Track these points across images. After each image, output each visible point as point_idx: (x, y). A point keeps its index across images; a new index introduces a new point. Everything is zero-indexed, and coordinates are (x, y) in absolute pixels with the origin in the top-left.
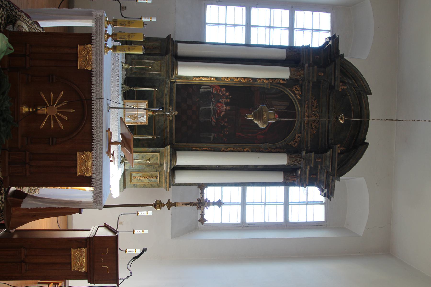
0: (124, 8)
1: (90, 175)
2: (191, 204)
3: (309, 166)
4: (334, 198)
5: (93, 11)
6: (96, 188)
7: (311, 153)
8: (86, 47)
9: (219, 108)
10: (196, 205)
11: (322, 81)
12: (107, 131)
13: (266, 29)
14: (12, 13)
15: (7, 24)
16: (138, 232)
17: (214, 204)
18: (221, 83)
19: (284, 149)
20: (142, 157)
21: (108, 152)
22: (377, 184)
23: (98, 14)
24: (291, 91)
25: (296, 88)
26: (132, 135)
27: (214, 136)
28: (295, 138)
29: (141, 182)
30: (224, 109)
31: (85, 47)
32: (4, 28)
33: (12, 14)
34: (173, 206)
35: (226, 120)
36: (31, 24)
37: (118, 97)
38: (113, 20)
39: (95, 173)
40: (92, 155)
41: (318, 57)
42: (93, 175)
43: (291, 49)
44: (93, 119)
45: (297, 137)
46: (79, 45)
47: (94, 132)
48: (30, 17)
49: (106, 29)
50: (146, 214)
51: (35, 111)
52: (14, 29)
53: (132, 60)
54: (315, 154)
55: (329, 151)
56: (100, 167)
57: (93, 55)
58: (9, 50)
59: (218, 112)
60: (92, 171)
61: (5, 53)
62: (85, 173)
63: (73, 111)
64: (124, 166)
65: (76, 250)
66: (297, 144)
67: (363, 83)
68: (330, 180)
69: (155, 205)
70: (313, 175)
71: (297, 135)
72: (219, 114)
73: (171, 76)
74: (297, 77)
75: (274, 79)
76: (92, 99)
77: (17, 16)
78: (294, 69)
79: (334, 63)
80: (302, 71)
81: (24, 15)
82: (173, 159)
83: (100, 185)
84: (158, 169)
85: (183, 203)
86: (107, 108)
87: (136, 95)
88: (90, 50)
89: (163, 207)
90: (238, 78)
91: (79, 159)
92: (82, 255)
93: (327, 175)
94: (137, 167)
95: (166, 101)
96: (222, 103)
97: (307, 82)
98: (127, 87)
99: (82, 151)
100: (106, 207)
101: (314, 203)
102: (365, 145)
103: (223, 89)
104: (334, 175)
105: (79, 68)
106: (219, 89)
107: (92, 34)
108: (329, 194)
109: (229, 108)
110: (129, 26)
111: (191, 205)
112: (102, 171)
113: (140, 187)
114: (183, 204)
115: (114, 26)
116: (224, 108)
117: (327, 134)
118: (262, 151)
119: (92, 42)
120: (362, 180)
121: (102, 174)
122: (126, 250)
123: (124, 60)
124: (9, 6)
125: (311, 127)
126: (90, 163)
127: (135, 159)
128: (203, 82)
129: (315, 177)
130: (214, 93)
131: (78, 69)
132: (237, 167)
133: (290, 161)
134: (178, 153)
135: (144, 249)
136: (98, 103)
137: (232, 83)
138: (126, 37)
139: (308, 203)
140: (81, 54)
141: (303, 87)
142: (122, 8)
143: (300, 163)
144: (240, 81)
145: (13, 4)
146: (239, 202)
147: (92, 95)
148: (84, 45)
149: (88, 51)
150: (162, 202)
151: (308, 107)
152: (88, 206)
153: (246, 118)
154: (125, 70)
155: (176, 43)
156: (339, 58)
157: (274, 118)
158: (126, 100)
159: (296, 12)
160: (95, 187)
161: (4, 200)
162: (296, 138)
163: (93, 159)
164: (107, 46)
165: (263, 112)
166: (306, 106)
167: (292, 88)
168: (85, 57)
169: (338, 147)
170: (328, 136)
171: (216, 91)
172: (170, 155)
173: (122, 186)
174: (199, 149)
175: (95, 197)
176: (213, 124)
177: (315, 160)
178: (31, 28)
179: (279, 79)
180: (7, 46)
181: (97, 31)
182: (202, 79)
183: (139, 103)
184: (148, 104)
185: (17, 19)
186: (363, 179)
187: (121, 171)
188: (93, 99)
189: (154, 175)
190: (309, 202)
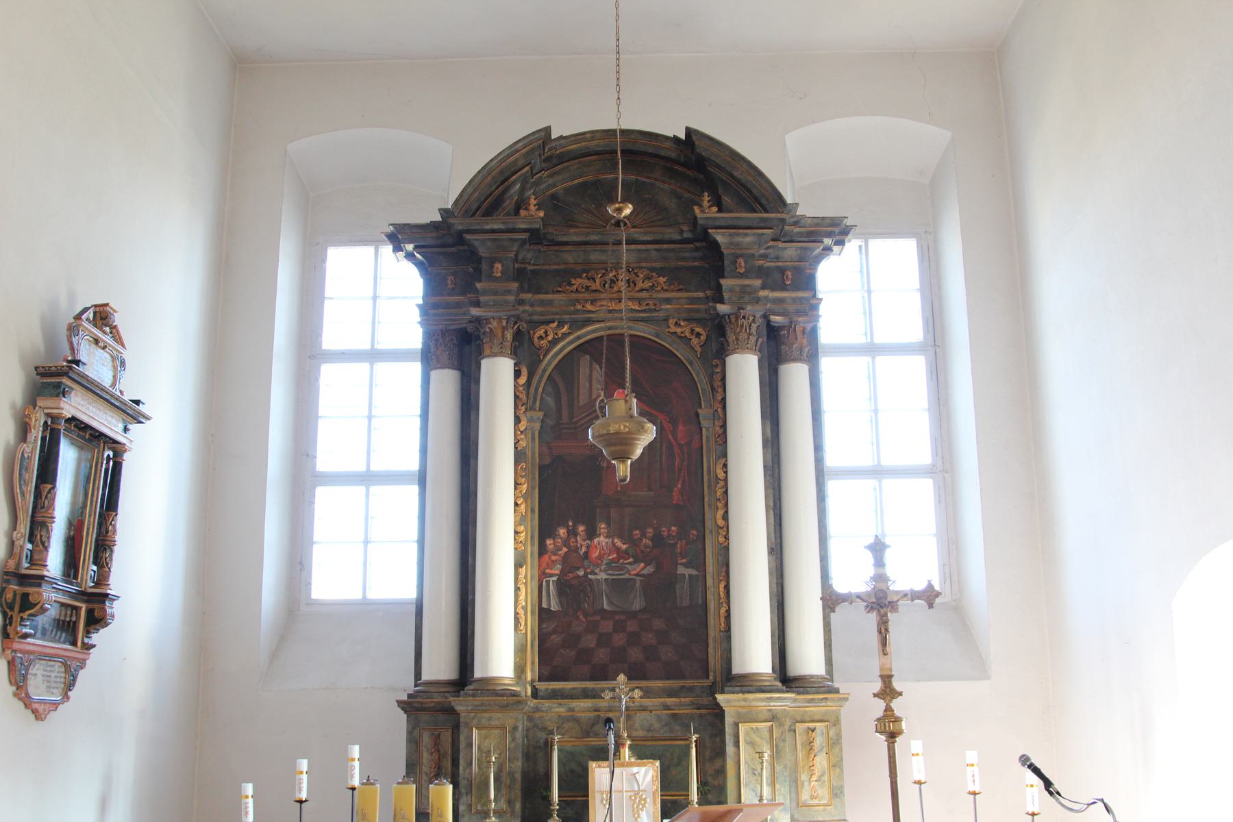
7: (724, 288)
10: (886, 615)
18: (531, 550)
25: (541, 338)
27: (686, 566)
34: (890, 682)
41: (450, 279)
45: (679, 330)
50: (921, 758)
54: (723, 277)
59: (614, 558)
66: (698, 330)
68: (797, 230)
71: (673, 329)
84: (787, 727)
106: (550, 558)
111: (887, 630)
117: (665, 246)
128: (532, 605)
134: (736, 670)
135: (1023, 765)
137: (532, 520)
141: (535, 318)
143: (751, 318)
151: (593, 302)
156: (451, 221)
157: (626, 401)
166: (589, 307)
176: (650, 569)
177: (741, 276)
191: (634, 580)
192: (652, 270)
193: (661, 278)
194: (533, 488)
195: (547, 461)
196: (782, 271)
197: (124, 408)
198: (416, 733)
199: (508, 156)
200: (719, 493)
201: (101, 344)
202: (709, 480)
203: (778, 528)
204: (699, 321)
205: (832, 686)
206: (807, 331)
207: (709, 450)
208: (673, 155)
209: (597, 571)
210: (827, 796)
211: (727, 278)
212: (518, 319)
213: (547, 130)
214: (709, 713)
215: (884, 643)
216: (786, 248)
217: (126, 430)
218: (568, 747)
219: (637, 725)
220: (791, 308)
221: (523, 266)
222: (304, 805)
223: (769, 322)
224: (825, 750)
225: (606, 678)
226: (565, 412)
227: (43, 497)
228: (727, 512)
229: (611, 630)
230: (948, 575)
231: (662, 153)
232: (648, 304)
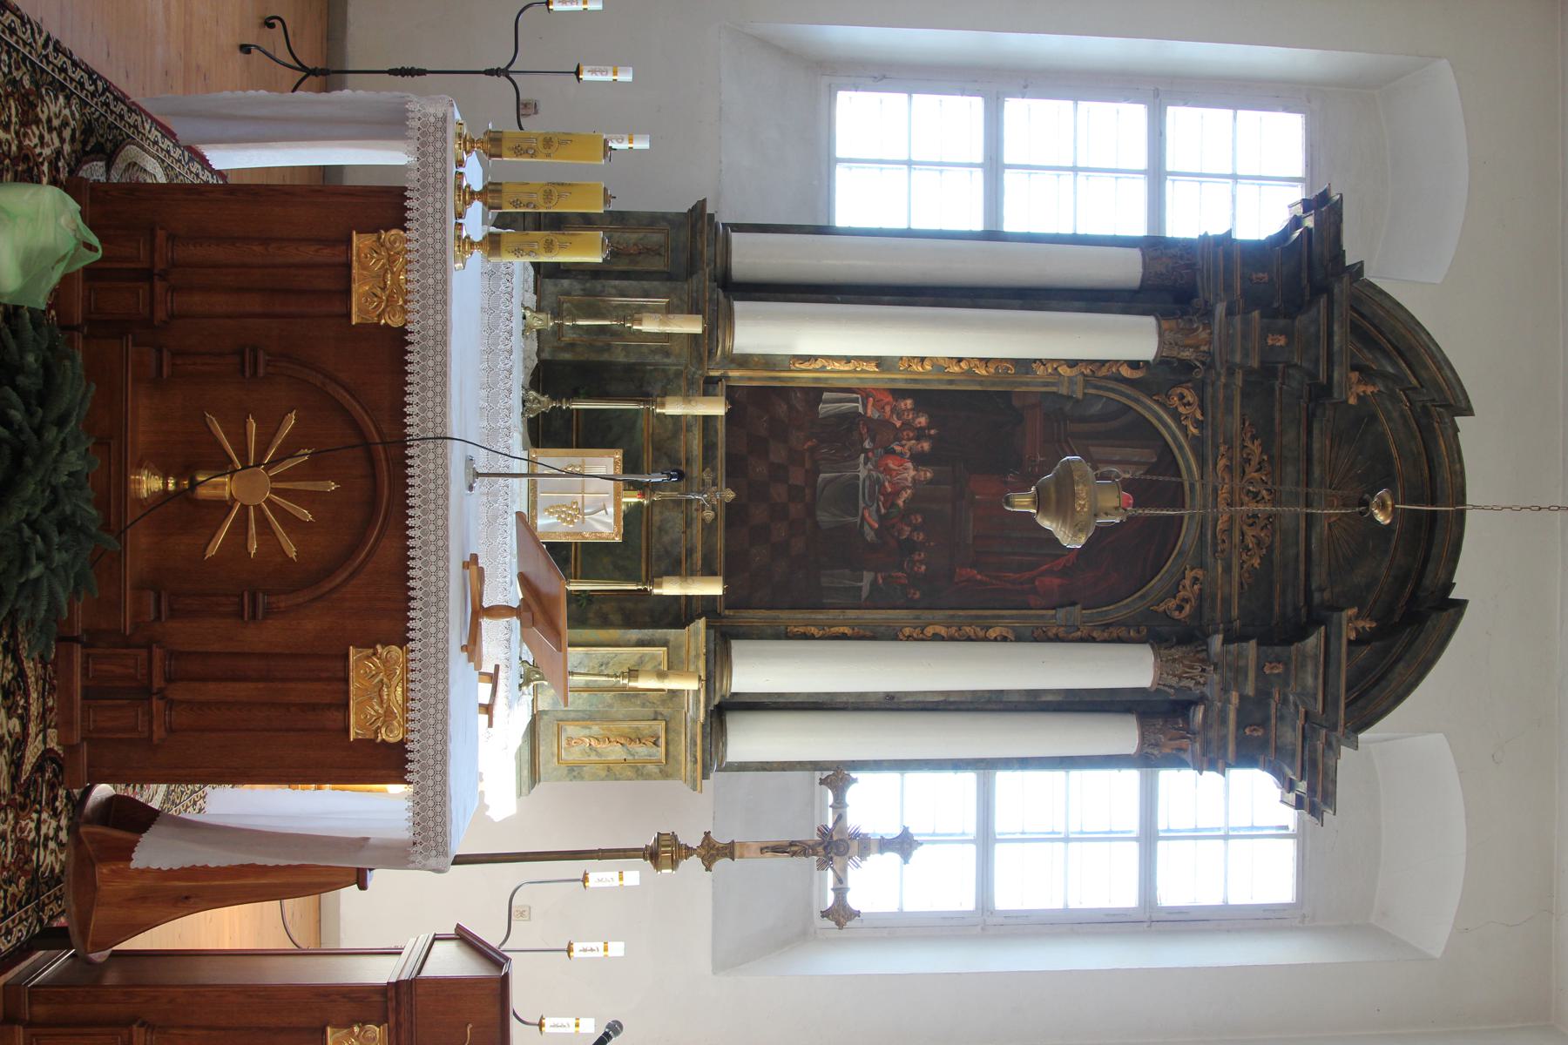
0: (528, 106)
1: (401, 736)
2: (794, 849)
3: (1237, 691)
4: (1335, 814)
5: (410, 101)
6: (423, 788)
7: (1244, 644)
8: (382, 240)
9: (891, 476)
10: (815, 854)
11: (1280, 366)
12: (466, 565)
13: (1058, 176)
14: (101, 114)
15: (81, 157)
16: (585, 950)
17: (885, 845)
18: (899, 379)
20: (602, 665)
21: (470, 648)
22: (1493, 756)
23: (431, 110)
25: (1182, 397)
26: (561, 579)
27: (874, 583)
28: (1181, 587)
29: (597, 758)
30: (910, 479)
31: (380, 238)
32: (71, 172)
33: (103, 119)
34: (725, 855)
35: (917, 520)
36: (179, 161)
38: (485, 134)
39: (419, 731)
40: (408, 661)
41: (1265, 276)
42: (410, 736)
43: (1154, 247)
44: (411, 517)
45: (1187, 582)
46: (354, 233)
47: (413, 568)
48: (175, 130)
49: (461, 170)
50: (616, 883)
51: (187, 487)
52: (112, 177)
53: (562, 298)
54: (1259, 644)
55: (1315, 635)
57: (410, 271)
58: (87, 251)
59: (885, 487)
60: (407, 720)
61: (69, 265)
62: (379, 728)
63: (333, 486)
64: (533, 700)
65: (345, 1031)
66: (1188, 607)
67: (1440, 372)
68: (1320, 745)
69: (652, 855)
70: (1251, 725)
71: (1189, 574)
73: (709, 357)
74: (1187, 354)
75: (1098, 364)
76: (408, 438)
77: (125, 126)
78: (1175, 321)
79: (1325, 296)
80: (1204, 329)
81: (151, 128)
82: (718, 669)
83: (438, 778)
84: (660, 709)
85: (763, 846)
86: (466, 475)
87: (577, 430)
88: (399, 249)
89: (684, 863)
90: (960, 360)
91: (358, 672)
93: (1306, 725)
94: (581, 701)
95: (688, 451)
96: (902, 454)
97: (1223, 371)
98: (542, 399)
99: (368, 642)
100: (460, 860)
101: (1253, 833)
102: (1452, 611)
103: (906, 405)
104: (1334, 727)
106: (888, 403)
107: (405, 189)
108: (1316, 799)
109: (928, 475)
110: (548, 156)
111: (794, 854)
112: (445, 723)
113: (595, 777)
114: (762, 849)
115: (491, 156)
117: (1302, 568)
118: (1056, 635)
119: (406, 220)
120: (1436, 743)
121: (445, 732)
122: (541, 1020)
123: (531, 300)
124: (92, 88)
125: (1243, 541)
126: (399, 689)
127: (572, 673)
128: (827, 379)
129: (1260, 734)
130: (870, 417)
131: (354, 323)
132: (963, 699)
133: (1165, 675)
134: (736, 646)
135: (609, 1026)
136: (431, 456)
137: (940, 381)
138: (538, 198)
139: (1231, 833)
140: (364, 267)
141: (1209, 390)
142: (521, 106)
143: (1202, 680)
144: (970, 373)
145: (106, 81)
146: (966, 832)
148: (376, 230)
149: (389, 254)
150: (682, 840)
151: (1229, 468)
152: (399, 856)
153: (1008, 509)
154: (535, 335)
155: (727, 232)
156: (1346, 279)
157: (1116, 508)
158: (538, 447)
159: (1171, 110)
160: (418, 783)
161: (68, 834)
162: (1184, 587)
163: (412, 676)
164: (464, 234)
165: (1073, 483)
166: (1222, 463)
167: (1168, 397)
168: (379, 276)
169: (1350, 620)
170: (1308, 575)
171: (878, 410)
172: (707, 654)
173: (526, 773)
174: (815, 633)
175: (419, 824)
176: (870, 535)
177: (1260, 668)
178: (177, 177)
179: (1118, 361)
180: (75, 236)
181: (424, 175)
182: (824, 367)
183: (588, 459)
184: (620, 464)
185: (124, 139)
186: (1439, 738)
187: (523, 717)
188: (410, 440)
189: (646, 732)
190: (1234, 829)
192: (1270, 549)
193: (1258, 561)
194: (981, 383)
195: (1016, 403)
196: (1264, 723)
199: (1433, 357)
203: (920, 706)
205: (711, 769)
208: (1427, 582)
209: (870, 466)
211: (1258, 649)
212: (1209, 366)
216: (1294, 730)
220: (1213, 734)
224: (629, 758)
225: (728, 475)
228: (943, 639)
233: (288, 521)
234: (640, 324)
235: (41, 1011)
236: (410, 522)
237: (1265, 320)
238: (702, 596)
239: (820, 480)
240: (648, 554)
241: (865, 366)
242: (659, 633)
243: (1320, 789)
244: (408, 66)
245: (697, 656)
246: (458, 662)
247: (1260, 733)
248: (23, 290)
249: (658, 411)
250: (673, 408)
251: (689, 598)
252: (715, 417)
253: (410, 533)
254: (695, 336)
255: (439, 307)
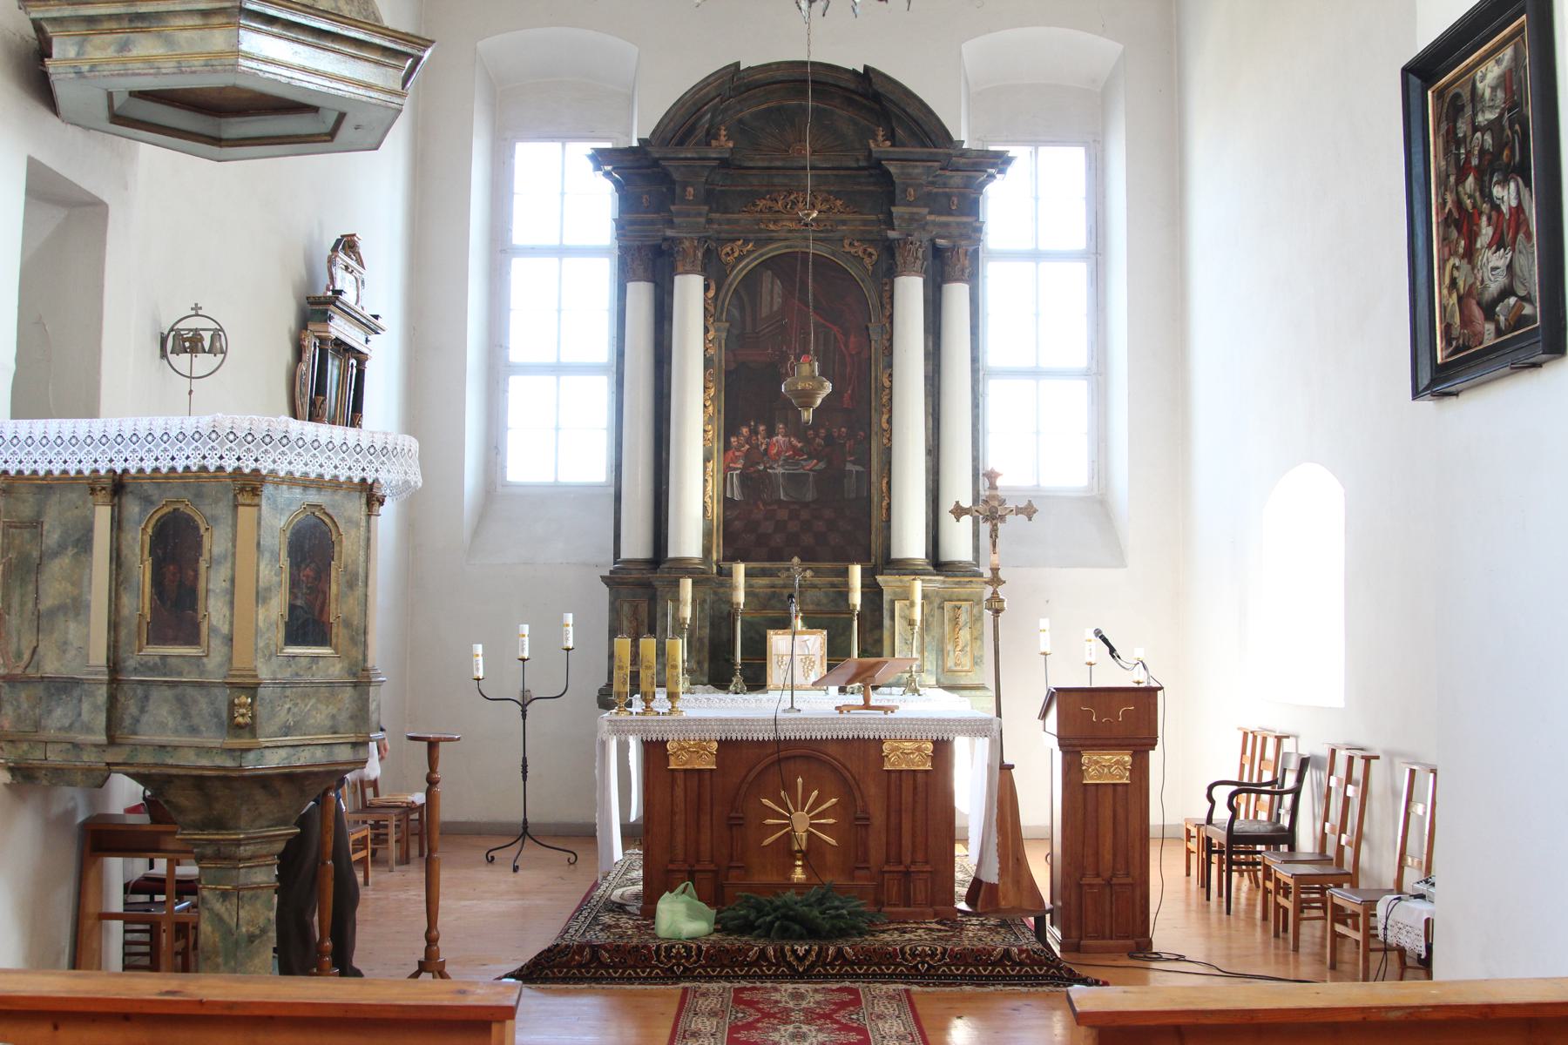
7: (894, 215)
10: (996, 525)
18: (717, 447)
19: (884, 282)
23: (606, 728)
24: (733, 267)
25: (728, 254)
27: (854, 463)
34: (997, 573)
37: (761, 700)
41: (645, 198)
42: (930, 738)
45: (853, 251)
50: (1047, 633)
54: (894, 205)
56: (914, 722)
59: (790, 455)
63: (800, 780)
66: (869, 250)
68: (964, 160)
71: (847, 249)
72: (797, 452)
78: (678, 263)
82: (907, 567)
84: (936, 605)
92: (1097, 762)
96: (767, 444)
100: (999, 714)
102: (872, 75)
104: (950, 156)
105: (715, 767)
106: (734, 453)
111: (996, 536)
112: (922, 720)
116: (780, 438)
117: (842, 172)
126: (906, 744)
128: (718, 494)
132: (931, 403)
134: (895, 555)
135: (1096, 636)
136: (785, 727)
137: (719, 419)
140: (686, 763)
141: (723, 235)
143: (918, 243)
147: (769, 740)
151: (775, 222)
152: (998, 746)
156: (649, 149)
157: (810, 365)
162: (856, 252)
163: (898, 737)
166: (772, 227)
176: (822, 465)
177: (910, 204)
189: (952, 614)
191: (808, 474)
192: (830, 193)
193: (838, 201)
194: (719, 391)
195: (733, 366)
196: (948, 196)
197: (368, 323)
198: (617, 603)
199: (701, 89)
200: (885, 399)
201: (350, 270)
202: (876, 387)
203: (936, 431)
204: (872, 242)
205: (977, 571)
206: (969, 253)
207: (876, 360)
208: (852, 86)
209: (775, 466)
210: (969, 664)
211: (899, 206)
212: (706, 239)
213: (737, 64)
214: (870, 592)
215: (994, 545)
216: (952, 177)
217: (367, 341)
218: (748, 617)
219: (808, 600)
220: (955, 232)
221: (711, 187)
222: (570, 652)
223: (934, 245)
224: (968, 625)
225: (781, 559)
226: (748, 320)
227: (318, 407)
228: (891, 417)
229: (786, 518)
230: (1096, 471)
231: (842, 84)
232: (825, 225)
233: (818, 802)
234: (686, 619)
235: (1074, 933)
236: (819, 738)
237: (676, 201)
238: (862, 577)
239: (785, 499)
240: (835, 613)
241: (709, 470)
242: (886, 606)
243: (992, 160)
244: (529, 769)
245: (901, 581)
246: (897, 715)
247: (955, 200)
248: (707, 920)
249: (742, 607)
250: (740, 597)
251: (863, 586)
252: (746, 569)
253: (824, 737)
254: (694, 584)
255: (708, 723)
